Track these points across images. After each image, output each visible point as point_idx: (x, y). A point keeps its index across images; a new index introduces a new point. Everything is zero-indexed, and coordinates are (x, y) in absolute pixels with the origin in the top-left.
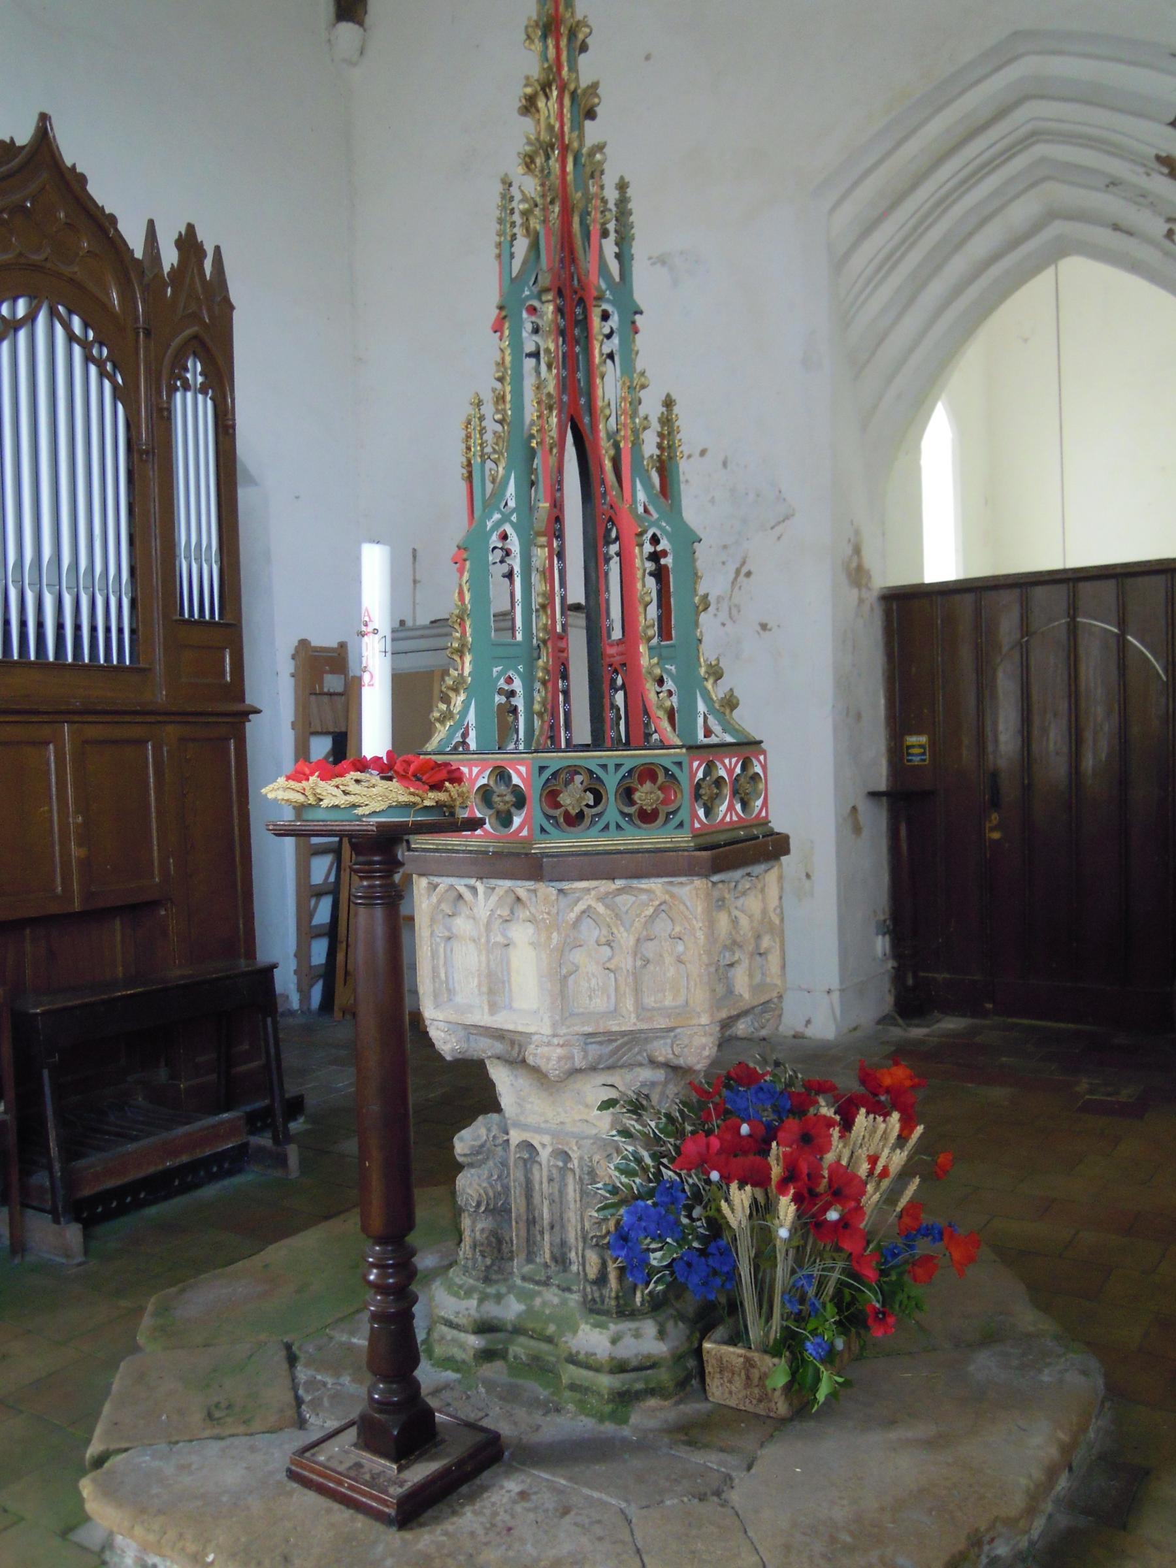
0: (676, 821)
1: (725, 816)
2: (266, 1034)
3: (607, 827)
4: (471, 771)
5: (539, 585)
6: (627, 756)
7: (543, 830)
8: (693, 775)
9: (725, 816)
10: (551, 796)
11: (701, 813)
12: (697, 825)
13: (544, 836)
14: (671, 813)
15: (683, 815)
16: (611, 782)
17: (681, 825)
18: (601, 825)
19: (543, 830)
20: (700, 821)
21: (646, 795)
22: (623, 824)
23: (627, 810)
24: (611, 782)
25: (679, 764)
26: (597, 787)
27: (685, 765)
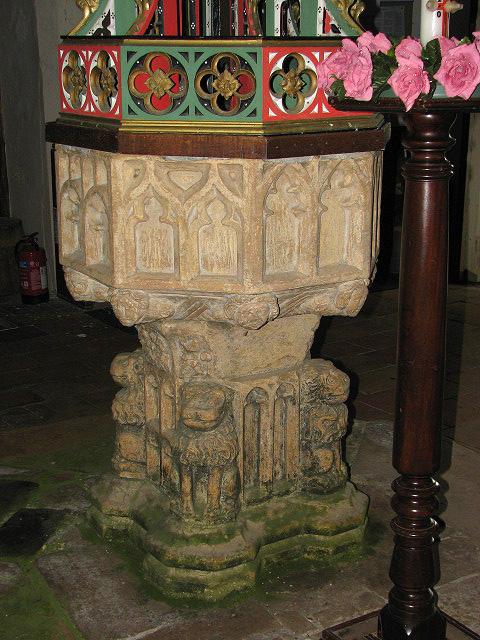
0: (249, 110)
1: (93, 56)
2: (46, 169)
3: (187, 111)
4: (320, 108)
5: (279, 428)
6: (208, 45)
7: (130, 111)
8: (268, 65)
9: (93, 56)
10: (246, 84)
11: (279, 103)
12: (271, 113)
13: (132, 116)
14: (246, 101)
15: (257, 103)
16: (191, 68)
17: (254, 112)
18: (182, 108)
19: (130, 111)
20: (276, 109)
21: (228, 84)
22: (201, 109)
23: (206, 96)
24: (191, 68)
25: (254, 55)
26: (202, 91)
27: (260, 57)
